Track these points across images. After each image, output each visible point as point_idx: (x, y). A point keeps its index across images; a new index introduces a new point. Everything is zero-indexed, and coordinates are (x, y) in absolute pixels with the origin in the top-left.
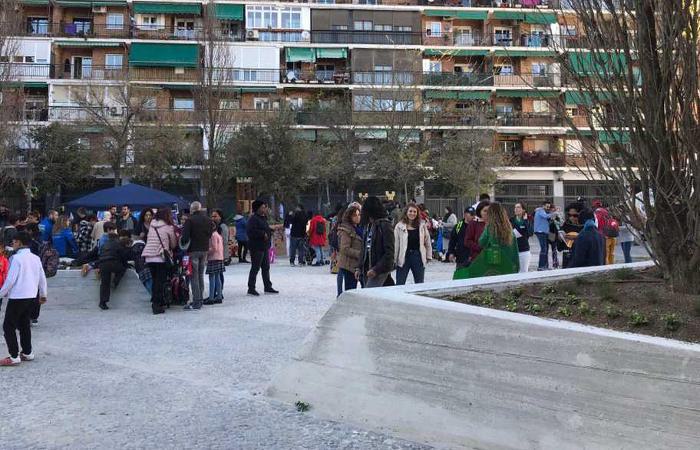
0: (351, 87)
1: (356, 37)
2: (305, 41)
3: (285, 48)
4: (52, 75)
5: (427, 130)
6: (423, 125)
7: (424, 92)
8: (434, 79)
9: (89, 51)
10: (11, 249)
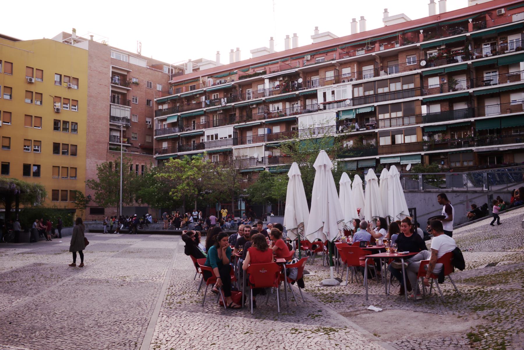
0: (376, 131)
1: (380, 98)
2: (349, 105)
3: (339, 111)
4: (234, 144)
5: (425, 154)
6: (423, 150)
7: (423, 128)
8: (430, 117)
9: (250, 128)
10: (202, 245)
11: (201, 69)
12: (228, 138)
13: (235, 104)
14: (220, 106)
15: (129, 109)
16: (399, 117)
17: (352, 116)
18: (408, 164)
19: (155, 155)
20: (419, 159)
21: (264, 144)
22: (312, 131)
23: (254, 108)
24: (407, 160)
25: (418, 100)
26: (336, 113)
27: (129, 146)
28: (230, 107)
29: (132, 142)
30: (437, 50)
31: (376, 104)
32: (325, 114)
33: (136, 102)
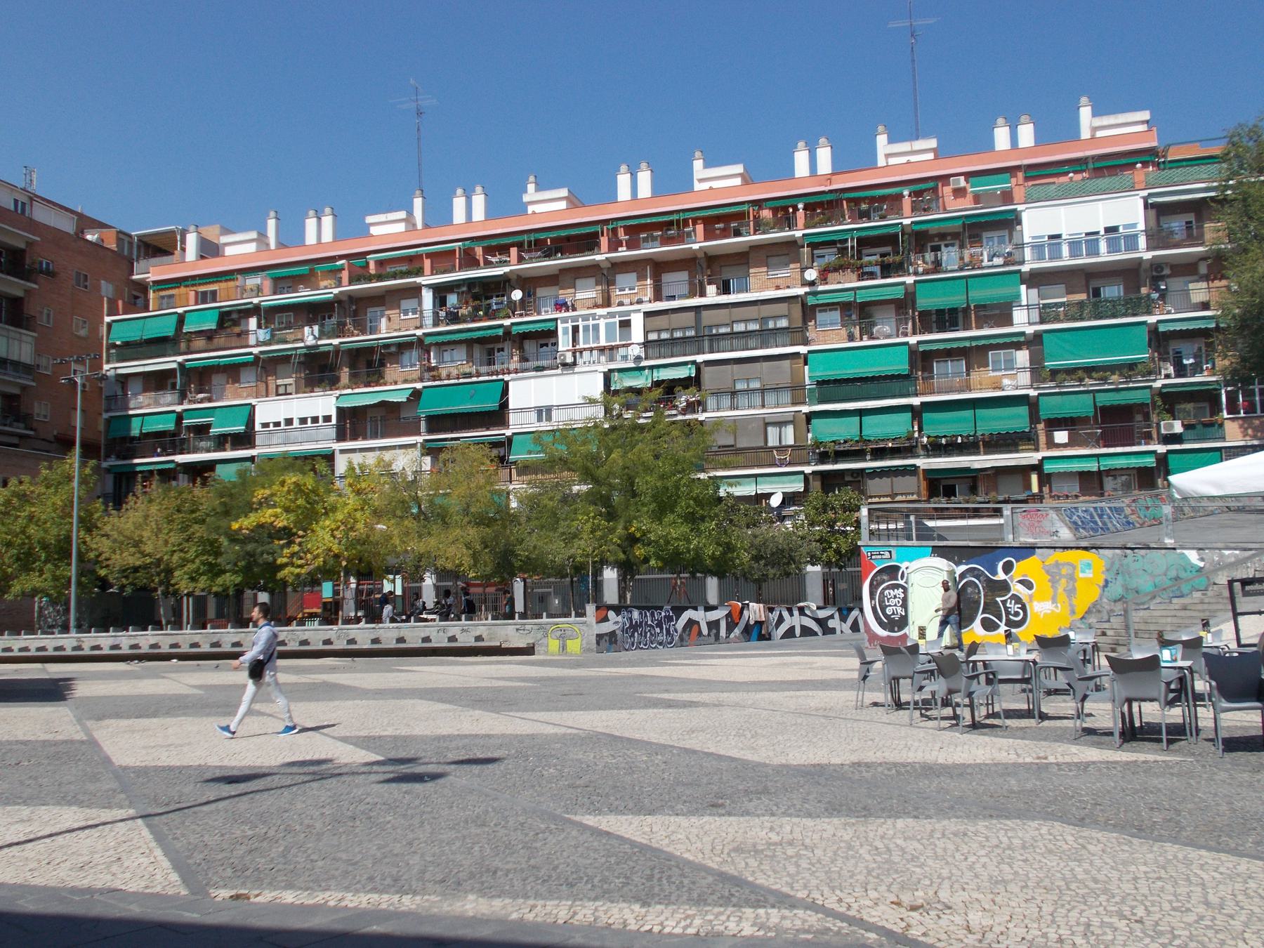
3: (611, 371)
4: (341, 437)
5: (814, 473)
11: (229, 251)
12: (283, 426)
13: (341, 343)
14: (302, 345)
15: (30, 339)
16: (753, 390)
17: (641, 381)
18: (773, 494)
19: (105, 460)
20: (800, 482)
21: (420, 439)
22: (544, 412)
23: (390, 354)
24: (772, 483)
25: (798, 354)
26: (604, 373)
27: (28, 436)
28: (326, 349)
29: (35, 425)
30: (835, 250)
31: (700, 358)
32: (554, 378)
33: (48, 322)
